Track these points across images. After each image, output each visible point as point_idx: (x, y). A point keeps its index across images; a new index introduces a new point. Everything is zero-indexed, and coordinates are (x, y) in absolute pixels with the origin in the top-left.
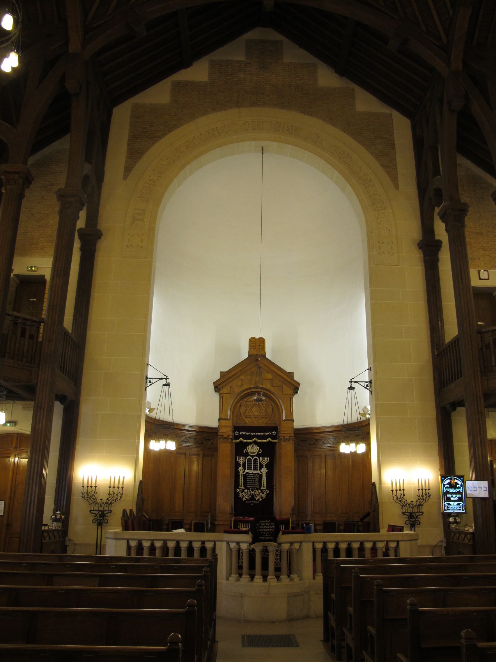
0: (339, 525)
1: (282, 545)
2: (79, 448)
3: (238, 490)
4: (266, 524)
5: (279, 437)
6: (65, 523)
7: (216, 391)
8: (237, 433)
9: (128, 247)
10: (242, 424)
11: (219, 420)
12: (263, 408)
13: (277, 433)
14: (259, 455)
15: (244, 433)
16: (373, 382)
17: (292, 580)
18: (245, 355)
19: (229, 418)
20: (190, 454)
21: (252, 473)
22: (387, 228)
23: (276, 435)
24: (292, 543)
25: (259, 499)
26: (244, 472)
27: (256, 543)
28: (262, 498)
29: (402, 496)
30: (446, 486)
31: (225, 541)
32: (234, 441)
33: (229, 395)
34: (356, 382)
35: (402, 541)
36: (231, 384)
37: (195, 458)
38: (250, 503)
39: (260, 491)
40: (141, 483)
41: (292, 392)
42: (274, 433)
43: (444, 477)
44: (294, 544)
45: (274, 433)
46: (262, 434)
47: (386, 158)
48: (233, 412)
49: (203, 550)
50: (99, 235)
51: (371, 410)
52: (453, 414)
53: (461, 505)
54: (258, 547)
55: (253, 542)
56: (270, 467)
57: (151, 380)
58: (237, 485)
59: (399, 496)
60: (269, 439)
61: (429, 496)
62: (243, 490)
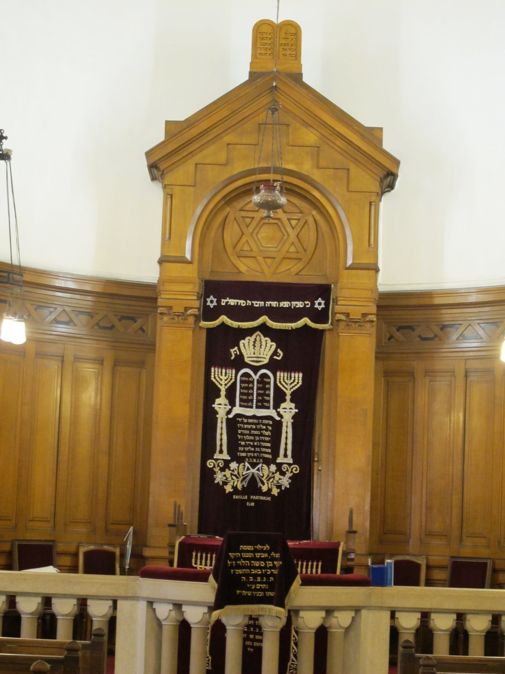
0: (495, 571)
1: (302, 614)
3: (210, 464)
4: (258, 555)
5: (334, 314)
7: (153, 178)
8: (212, 302)
10: (226, 275)
11: (161, 262)
12: (289, 229)
13: (327, 304)
14: (273, 365)
15: (232, 302)
18: (238, 71)
19: (188, 256)
20: (77, 359)
21: (254, 417)
23: (326, 310)
24: (329, 611)
25: (270, 490)
26: (229, 412)
27: (228, 608)
28: (279, 487)
31: (143, 598)
32: (205, 324)
33: (191, 189)
36: (197, 158)
37: (89, 370)
38: (245, 501)
39: (273, 468)
41: (375, 187)
42: (319, 304)
44: (336, 614)
45: (319, 304)
46: (285, 304)
48: (202, 242)
49: (81, 620)
54: (234, 618)
55: (221, 602)
56: (306, 399)
58: (208, 447)
60: (305, 321)
62: (227, 464)
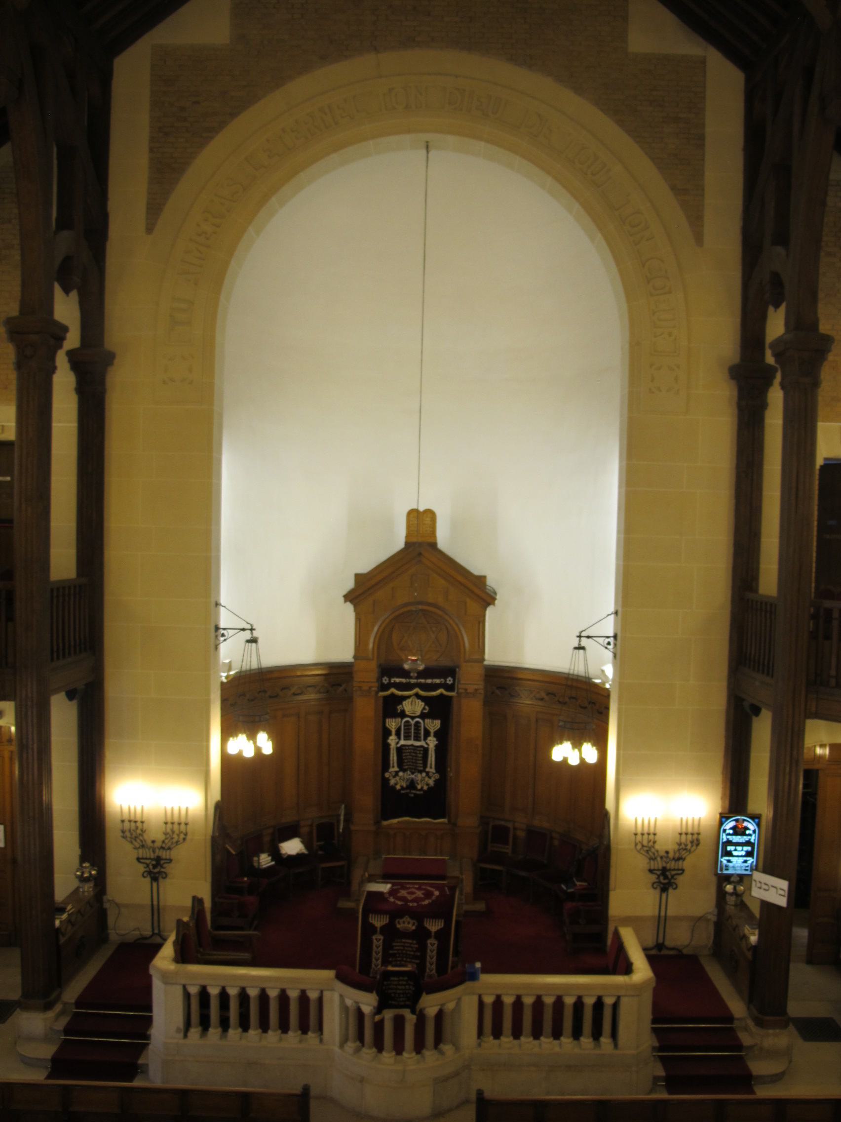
2: (109, 755)
3: (387, 775)
6: (100, 882)
8: (385, 680)
9: (164, 382)
13: (454, 681)
14: (423, 716)
15: (398, 680)
16: (619, 638)
17: (442, 1053)
18: (399, 543)
22: (670, 335)
23: (453, 685)
25: (422, 788)
26: (398, 743)
29: (651, 844)
30: (728, 832)
32: (382, 694)
34: (588, 637)
35: (625, 996)
39: (424, 774)
40: (218, 807)
42: (449, 681)
43: (724, 817)
45: (449, 681)
46: (429, 681)
47: (683, 172)
50: (109, 358)
51: (613, 680)
52: (754, 719)
53: (749, 862)
54: (388, 1015)
56: (442, 735)
57: (225, 632)
58: (386, 765)
59: (646, 842)
60: (441, 691)
61: (698, 845)
